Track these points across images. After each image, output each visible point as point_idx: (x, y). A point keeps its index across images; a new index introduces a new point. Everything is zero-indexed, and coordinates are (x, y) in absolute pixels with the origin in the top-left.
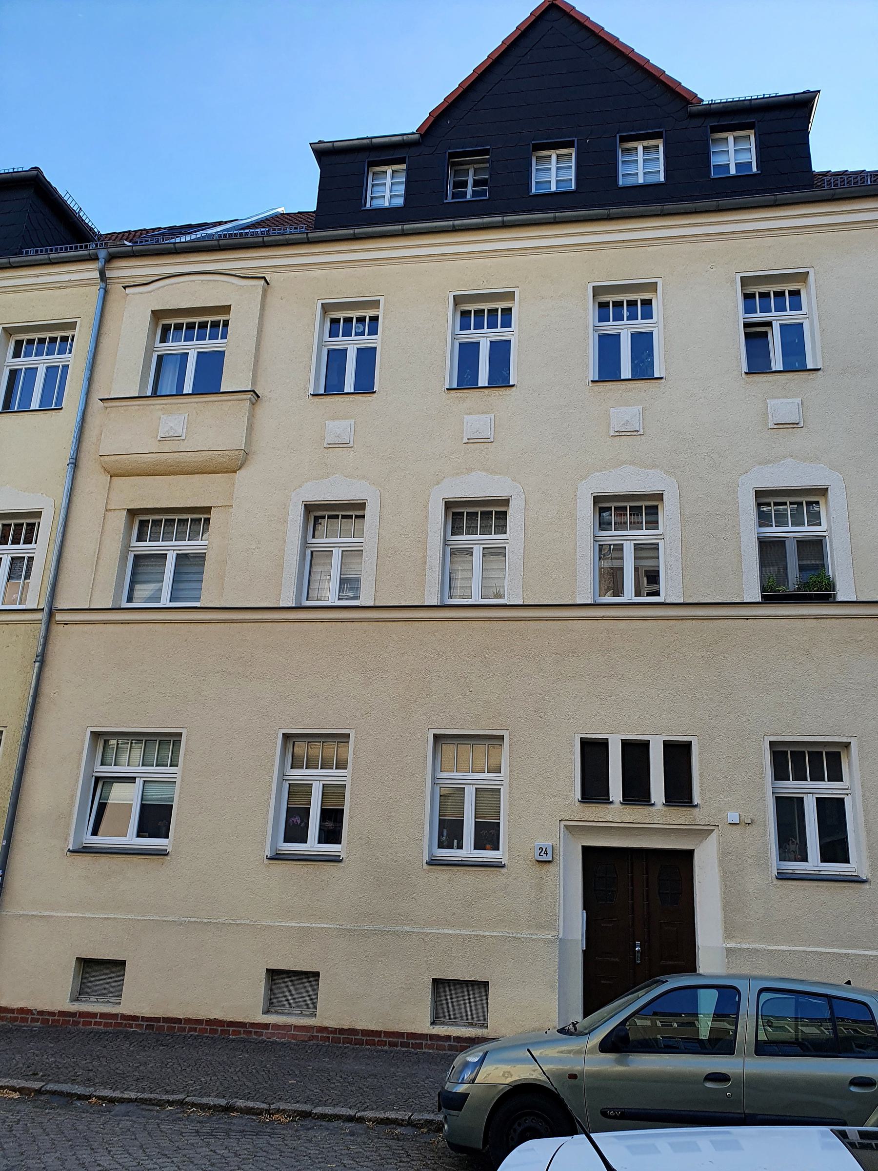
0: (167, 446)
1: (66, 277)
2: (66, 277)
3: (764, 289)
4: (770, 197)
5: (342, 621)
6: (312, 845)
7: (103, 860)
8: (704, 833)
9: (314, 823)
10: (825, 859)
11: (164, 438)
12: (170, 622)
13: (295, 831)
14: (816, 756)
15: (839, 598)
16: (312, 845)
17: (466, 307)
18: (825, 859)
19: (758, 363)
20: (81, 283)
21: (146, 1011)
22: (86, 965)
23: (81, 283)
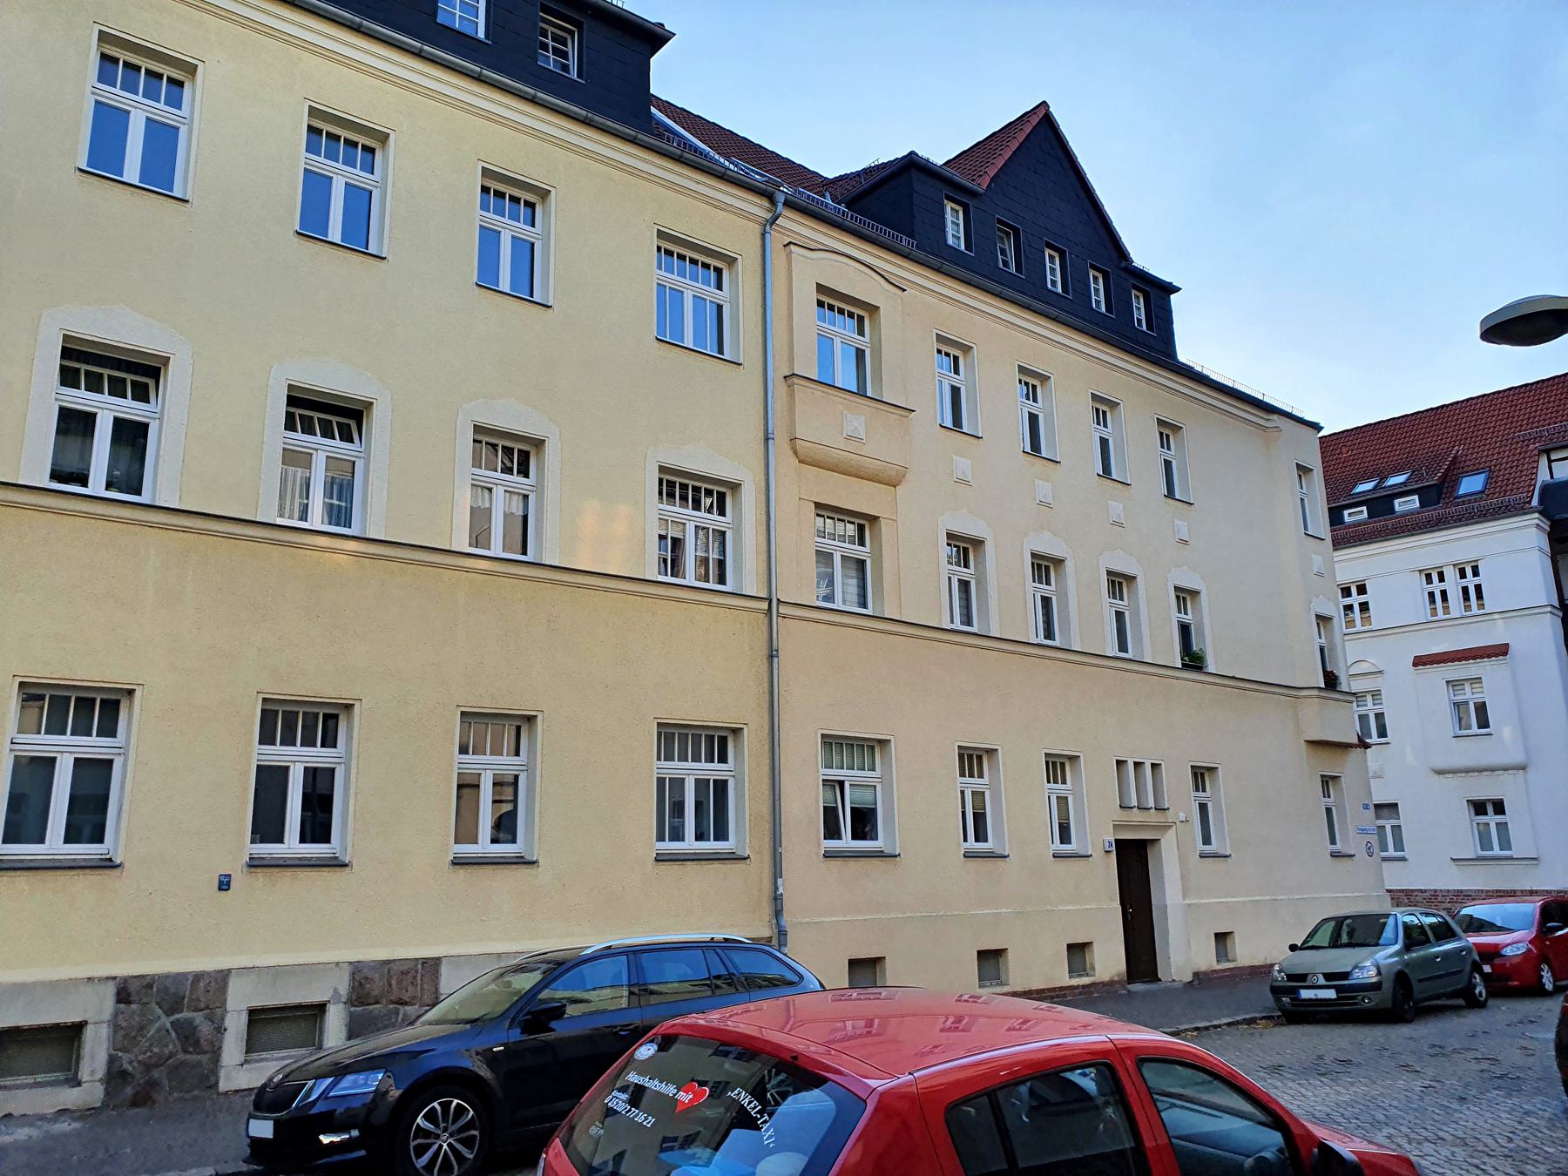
0: (852, 447)
1: (646, 167)
2: (646, 167)
3: (134, 59)
4: (998, 288)
5: (1068, 661)
6: (292, 845)
7: (852, 863)
8: (1165, 827)
9: (296, 811)
10: (854, 837)
11: (849, 438)
12: (911, 636)
13: (267, 825)
14: (85, 704)
15: (1211, 669)
16: (292, 845)
17: (113, 51)
18: (854, 837)
19: (312, 226)
20: (749, 217)
21: (1106, 978)
22: (854, 964)
23: (749, 217)
